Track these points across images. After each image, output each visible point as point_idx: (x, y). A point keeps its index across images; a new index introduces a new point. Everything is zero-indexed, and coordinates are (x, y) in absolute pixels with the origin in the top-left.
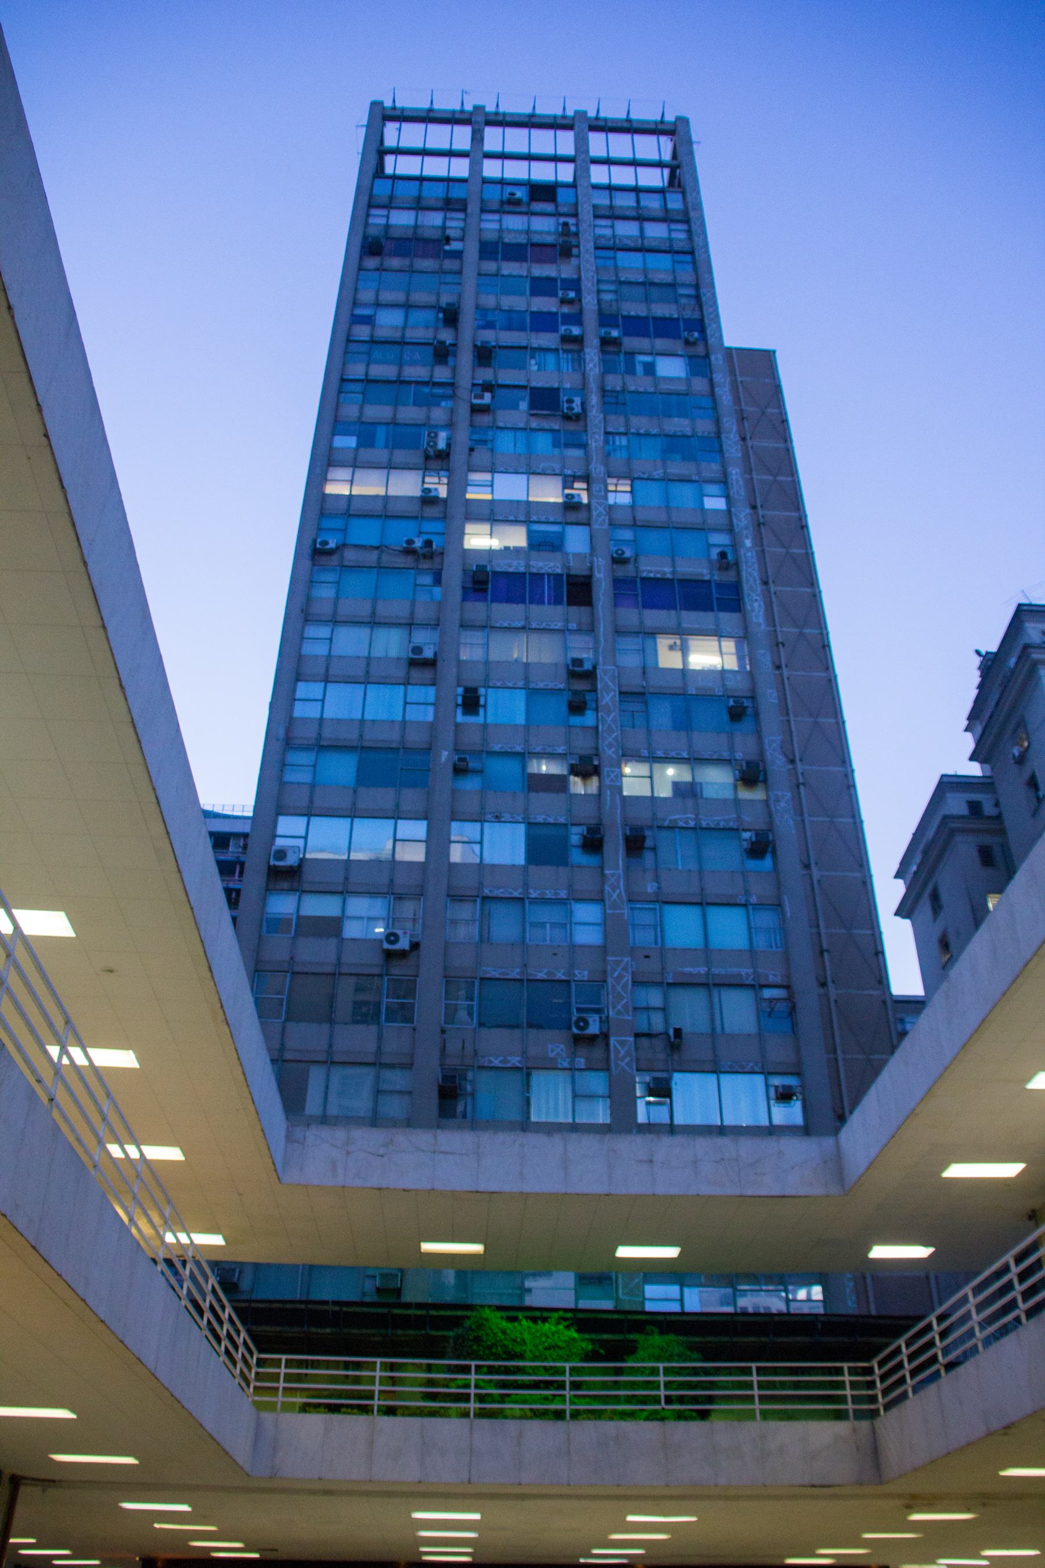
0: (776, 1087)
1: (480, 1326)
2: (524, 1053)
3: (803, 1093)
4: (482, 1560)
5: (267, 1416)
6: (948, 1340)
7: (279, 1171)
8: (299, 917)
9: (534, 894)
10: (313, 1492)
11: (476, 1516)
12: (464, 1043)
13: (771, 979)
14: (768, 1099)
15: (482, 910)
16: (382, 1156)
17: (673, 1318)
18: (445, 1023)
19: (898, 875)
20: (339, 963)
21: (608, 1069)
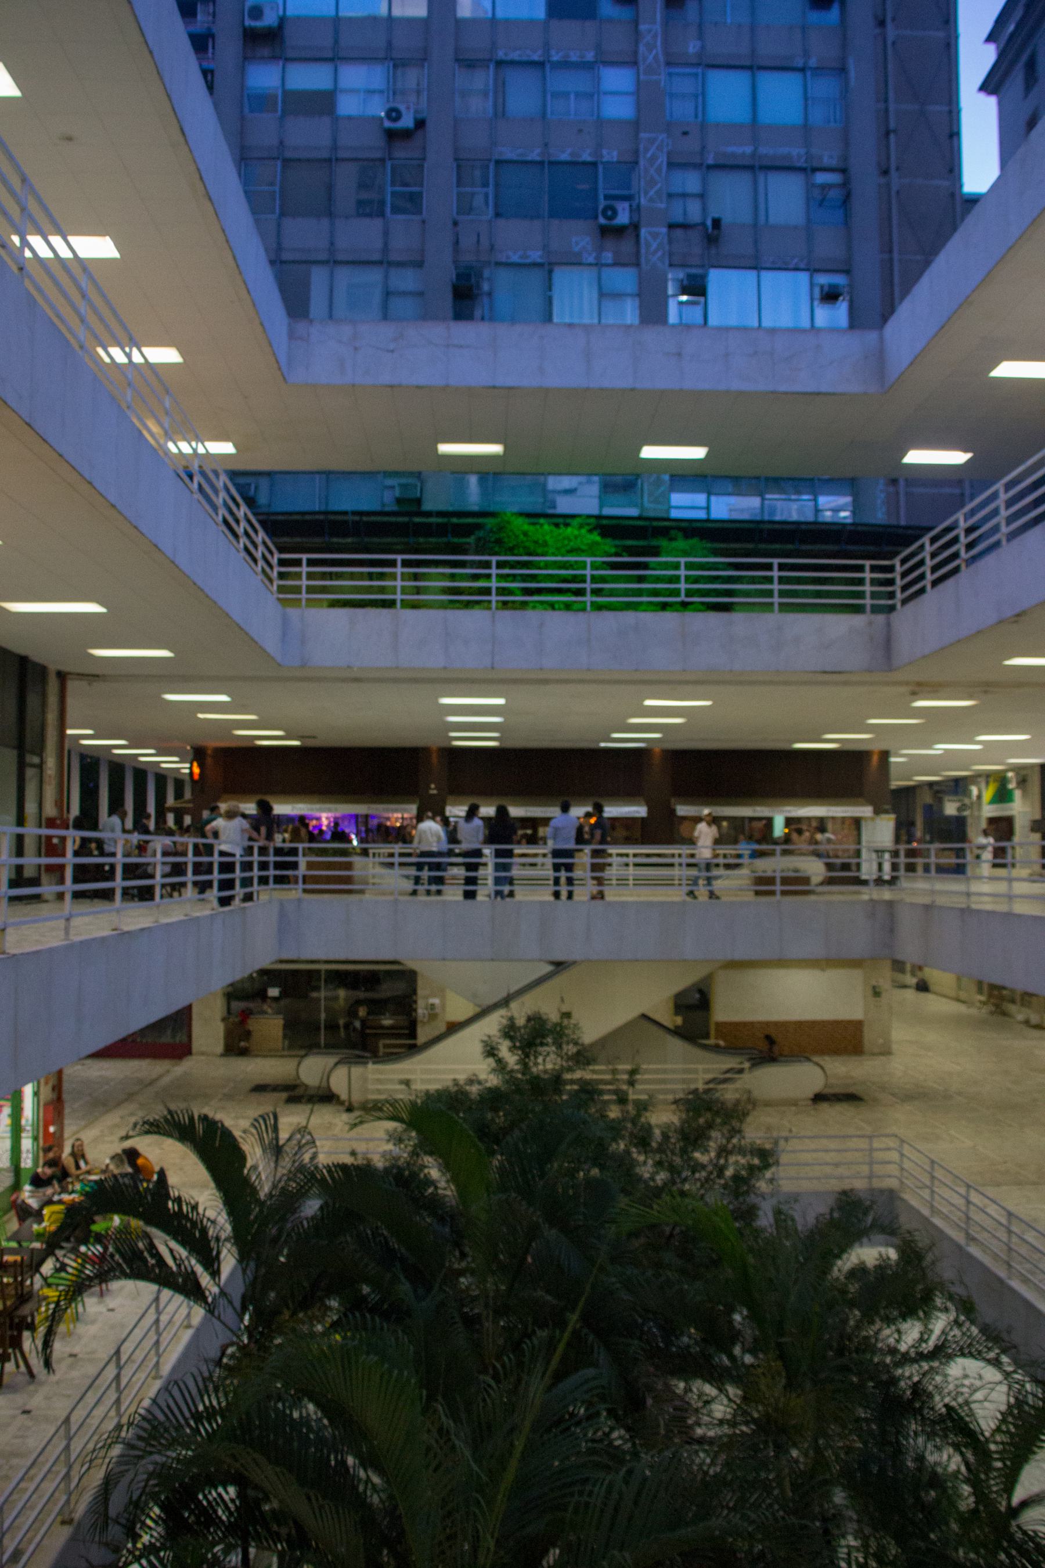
0: (822, 287)
1: (501, 528)
2: (545, 247)
3: (851, 293)
4: (510, 744)
5: (293, 613)
6: (974, 551)
7: (284, 369)
8: (285, 93)
9: (555, 57)
10: (344, 680)
11: (501, 701)
12: (479, 235)
13: (826, 161)
14: (812, 300)
15: (496, 80)
16: (392, 351)
17: (698, 525)
18: (458, 213)
19: (990, 38)
20: (335, 147)
21: (638, 265)
